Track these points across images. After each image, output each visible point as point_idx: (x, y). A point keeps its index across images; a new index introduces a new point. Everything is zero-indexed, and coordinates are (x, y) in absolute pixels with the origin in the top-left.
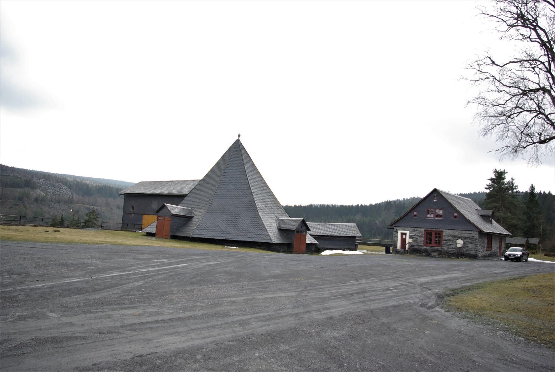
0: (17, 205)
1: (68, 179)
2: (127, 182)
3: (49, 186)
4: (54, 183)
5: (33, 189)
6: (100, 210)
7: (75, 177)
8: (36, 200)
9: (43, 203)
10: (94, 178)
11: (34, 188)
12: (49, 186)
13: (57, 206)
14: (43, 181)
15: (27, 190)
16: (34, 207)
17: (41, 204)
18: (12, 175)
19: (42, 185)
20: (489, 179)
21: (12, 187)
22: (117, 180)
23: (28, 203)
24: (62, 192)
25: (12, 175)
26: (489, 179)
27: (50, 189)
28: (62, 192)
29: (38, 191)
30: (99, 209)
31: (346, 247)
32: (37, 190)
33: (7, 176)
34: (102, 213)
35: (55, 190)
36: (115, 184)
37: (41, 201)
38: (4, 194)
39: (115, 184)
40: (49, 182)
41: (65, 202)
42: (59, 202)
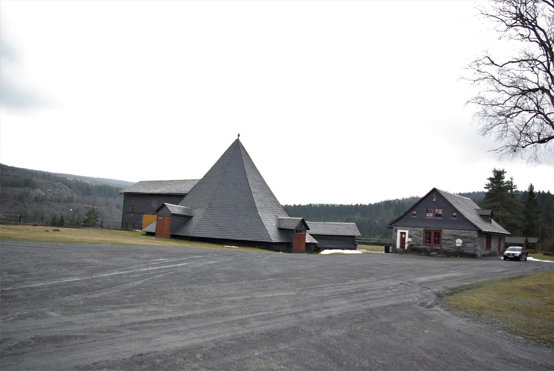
0: (17, 204)
1: (68, 178)
2: (127, 182)
3: (49, 186)
4: (54, 183)
5: (33, 189)
6: (100, 209)
7: (75, 177)
8: (36, 199)
9: (43, 203)
10: (94, 178)
11: (34, 187)
12: (49, 186)
13: (57, 206)
14: (43, 181)
15: (27, 189)
16: (34, 206)
17: (41, 203)
18: (12, 175)
19: (42, 185)
20: (488, 179)
21: (12, 187)
22: (117, 179)
23: (28, 202)
24: (62, 191)
25: (12, 175)
26: (488, 179)
27: (49, 189)
28: (62, 191)
29: (38, 191)
30: (99, 209)
31: (346, 246)
32: (37, 189)
33: (7, 175)
34: (102, 213)
35: (55, 190)
36: (115, 183)
37: (41, 200)
38: (4, 194)
39: (115, 183)
40: (49, 182)
41: (65, 202)
42: (59, 202)
